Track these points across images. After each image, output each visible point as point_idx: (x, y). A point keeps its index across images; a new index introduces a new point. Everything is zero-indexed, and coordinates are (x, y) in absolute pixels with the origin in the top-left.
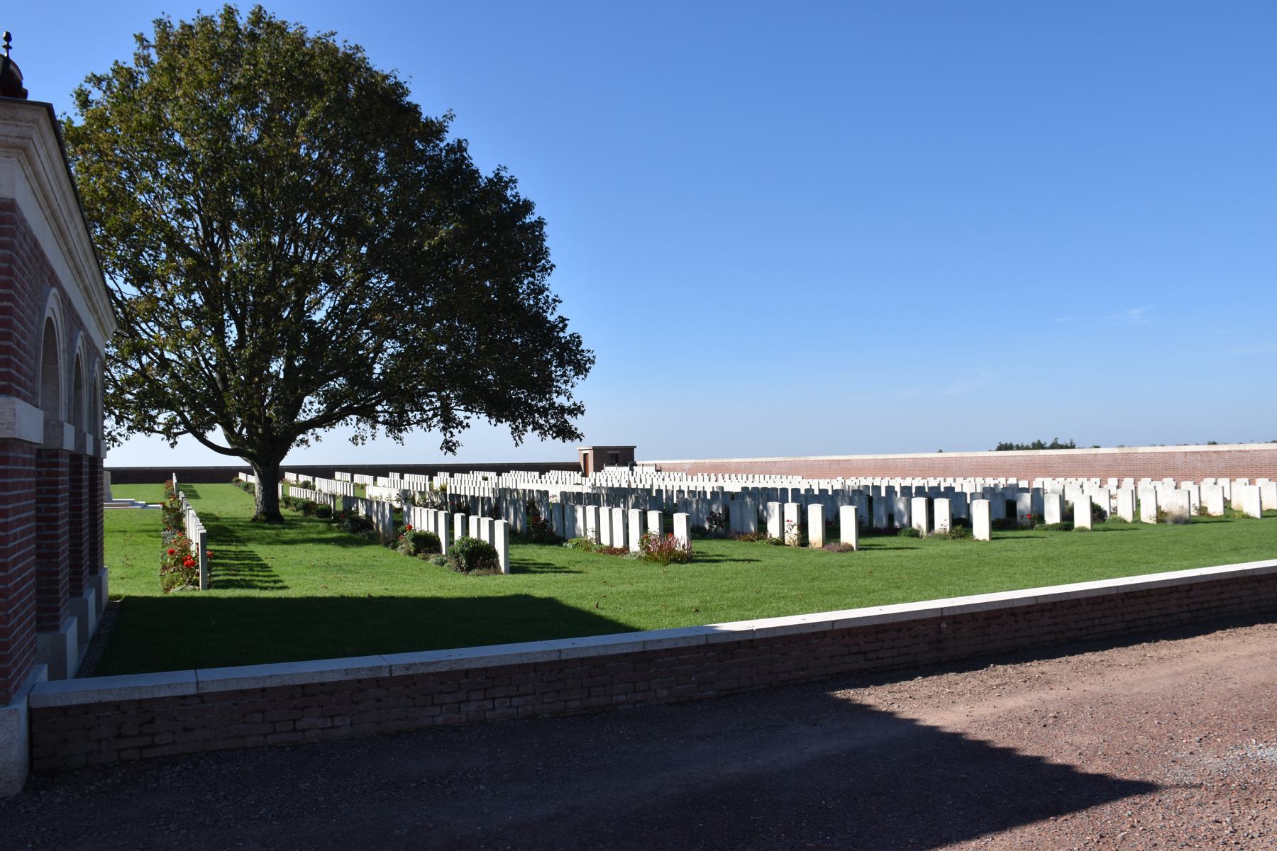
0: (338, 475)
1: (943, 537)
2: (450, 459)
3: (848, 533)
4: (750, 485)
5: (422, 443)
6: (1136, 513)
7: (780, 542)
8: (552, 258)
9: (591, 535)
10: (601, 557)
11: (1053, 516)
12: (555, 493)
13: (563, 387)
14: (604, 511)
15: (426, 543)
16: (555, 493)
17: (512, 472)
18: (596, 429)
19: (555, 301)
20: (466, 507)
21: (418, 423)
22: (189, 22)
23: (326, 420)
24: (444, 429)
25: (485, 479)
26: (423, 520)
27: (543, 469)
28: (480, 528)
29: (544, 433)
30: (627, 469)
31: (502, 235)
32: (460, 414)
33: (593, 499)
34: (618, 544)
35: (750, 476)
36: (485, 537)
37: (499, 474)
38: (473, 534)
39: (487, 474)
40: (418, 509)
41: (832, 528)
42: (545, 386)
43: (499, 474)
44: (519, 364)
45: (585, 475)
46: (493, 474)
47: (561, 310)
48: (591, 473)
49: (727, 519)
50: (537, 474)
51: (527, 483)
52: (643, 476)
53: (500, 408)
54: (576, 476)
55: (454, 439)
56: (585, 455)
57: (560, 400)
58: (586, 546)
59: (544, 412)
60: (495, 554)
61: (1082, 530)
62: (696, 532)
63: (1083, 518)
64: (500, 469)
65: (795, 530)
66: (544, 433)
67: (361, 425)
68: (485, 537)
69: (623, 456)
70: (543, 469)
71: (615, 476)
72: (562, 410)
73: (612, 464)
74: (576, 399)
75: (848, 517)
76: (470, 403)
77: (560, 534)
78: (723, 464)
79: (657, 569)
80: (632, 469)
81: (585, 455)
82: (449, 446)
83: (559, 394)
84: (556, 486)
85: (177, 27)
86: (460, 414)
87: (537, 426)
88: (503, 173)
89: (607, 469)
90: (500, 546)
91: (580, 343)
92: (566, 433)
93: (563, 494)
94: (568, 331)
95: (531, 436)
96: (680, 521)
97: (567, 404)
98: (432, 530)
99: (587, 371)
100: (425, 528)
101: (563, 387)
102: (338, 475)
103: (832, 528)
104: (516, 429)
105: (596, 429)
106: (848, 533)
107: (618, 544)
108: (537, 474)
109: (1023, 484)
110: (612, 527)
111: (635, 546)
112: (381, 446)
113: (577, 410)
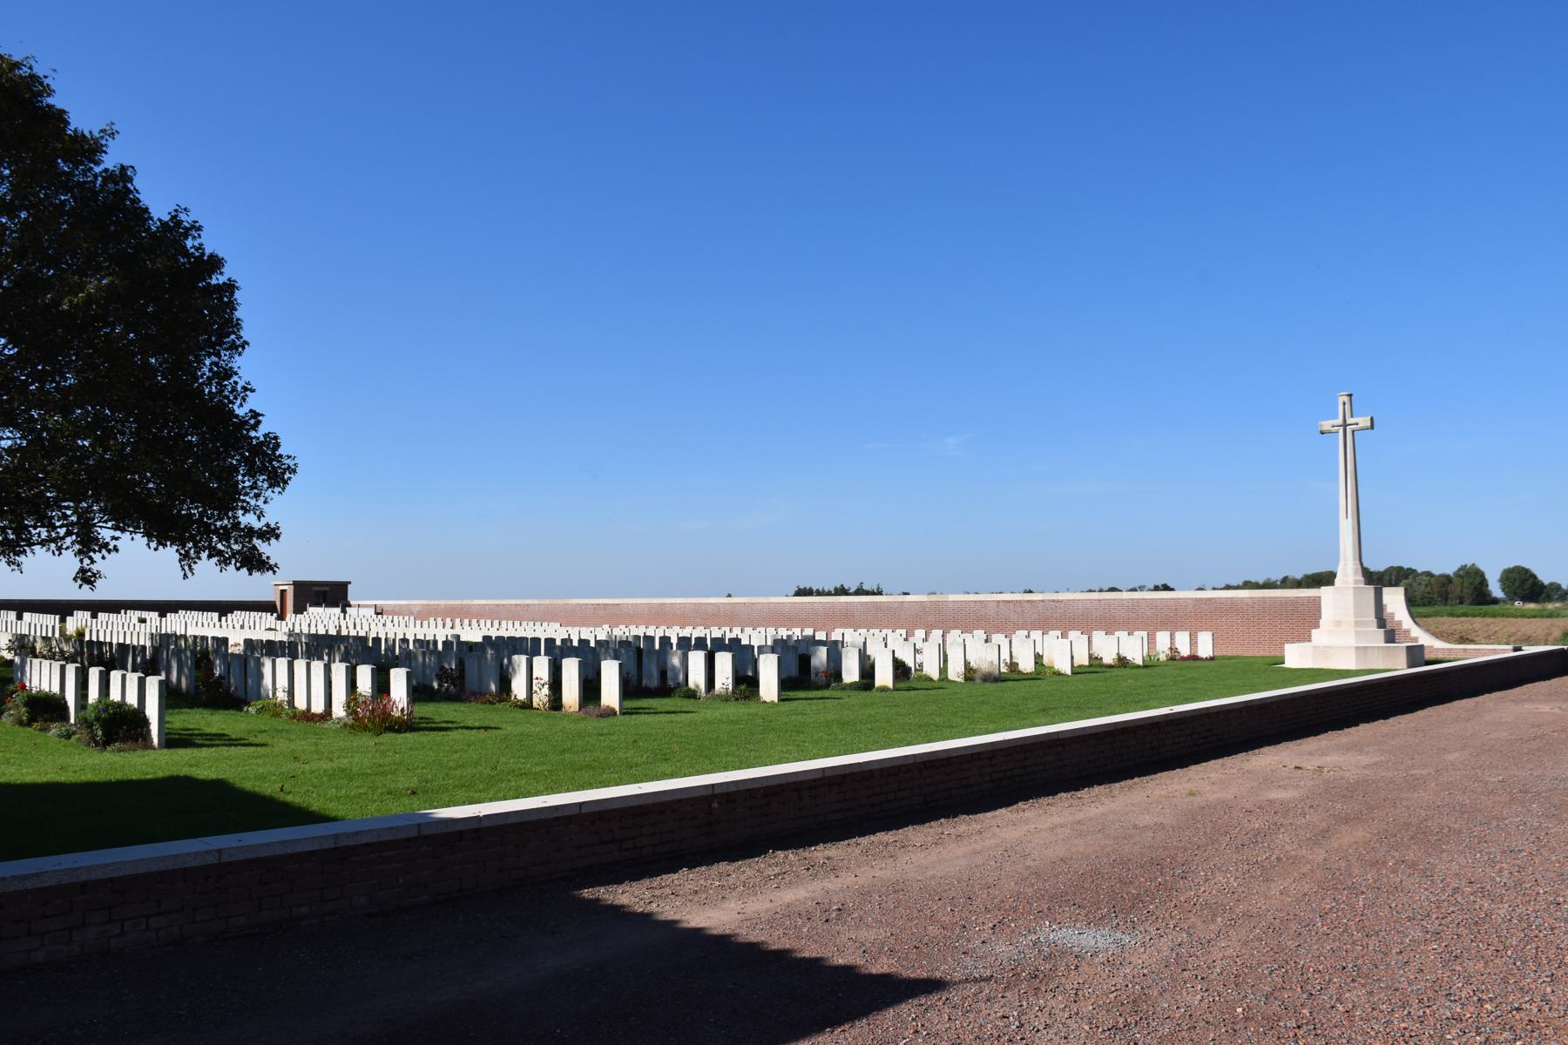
1: (725, 698)
2: (85, 594)
3: (610, 693)
4: (494, 634)
7: (527, 705)
9: (282, 696)
10: (296, 726)
11: (851, 673)
12: (1405, 626)
13: (253, 502)
14: (300, 665)
15: (47, 708)
18: (295, 559)
19: (245, 389)
25: (143, 621)
26: (43, 677)
28: (125, 688)
30: (337, 610)
31: (182, 299)
32: (106, 533)
34: (318, 707)
36: (132, 699)
37: (162, 615)
38: (115, 695)
39: (145, 614)
41: (591, 688)
42: (228, 499)
43: (162, 615)
44: (199, 475)
45: (281, 617)
47: (253, 402)
48: (290, 616)
49: (460, 676)
51: (203, 626)
52: (359, 621)
53: (162, 528)
54: (269, 619)
55: (95, 568)
56: (283, 592)
57: (247, 520)
58: (274, 710)
59: (225, 535)
60: (145, 722)
61: (884, 689)
62: (418, 692)
63: (884, 676)
65: (546, 690)
68: (132, 699)
69: (334, 594)
71: (322, 619)
72: (250, 532)
73: (318, 604)
74: (271, 518)
75: (610, 674)
76: (122, 522)
78: (462, 607)
79: (367, 740)
80: (344, 611)
83: (246, 511)
84: (238, 631)
88: (183, 217)
90: (152, 711)
91: (277, 446)
92: (254, 563)
93: (248, 642)
95: (206, 566)
96: (398, 681)
97: (257, 525)
98: (56, 689)
99: (286, 482)
101: (253, 502)
103: (591, 688)
104: (185, 556)
105: (295, 559)
106: (610, 693)
107: (318, 707)
109: (820, 636)
110: (311, 686)
111: (339, 711)
113: (270, 533)
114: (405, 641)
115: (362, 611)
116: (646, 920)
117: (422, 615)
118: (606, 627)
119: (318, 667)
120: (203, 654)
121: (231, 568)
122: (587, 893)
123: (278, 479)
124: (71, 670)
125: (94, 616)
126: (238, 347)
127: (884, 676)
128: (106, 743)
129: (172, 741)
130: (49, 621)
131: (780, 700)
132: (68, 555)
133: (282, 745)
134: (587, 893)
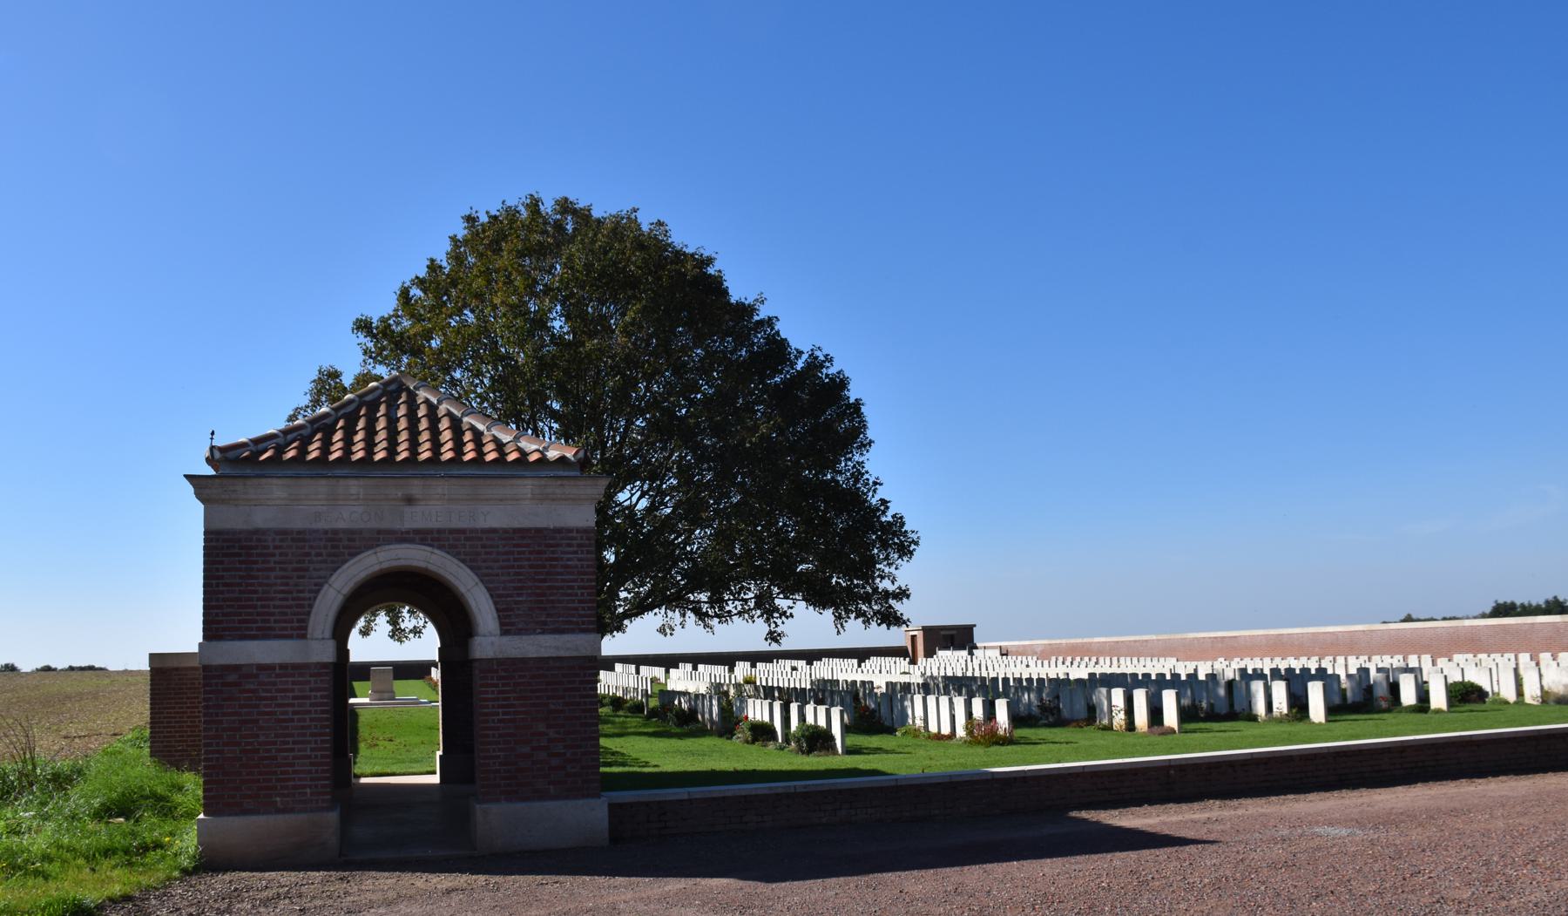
0: (618, 667)
1: (1281, 720)
2: (774, 647)
3: (1171, 717)
4: (1098, 670)
5: (744, 633)
6: (1520, 692)
7: (1109, 728)
8: (870, 434)
9: (919, 723)
10: (931, 743)
11: (1408, 696)
12: (880, 683)
13: (887, 570)
14: (931, 699)
15: (762, 732)
16: (880, 683)
17: (825, 660)
18: (919, 612)
19: (875, 483)
20: (788, 696)
21: (740, 614)
22: (494, 212)
23: (640, 608)
24: (767, 620)
25: (794, 669)
26: (757, 711)
27: (861, 655)
28: (816, 715)
29: (867, 622)
30: (964, 653)
31: (822, 413)
32: (782, 603)
33: (926, 688)
34: (946, 730)
35: (1115, 660)
36: (822, 723)
37: (810, 663)
38: (810, 720)
39: (795, 663)
40: (750, 701)
41: (1156, 713)
42: (867, 569)
43: (810, 663)
44: (840, 547)
45: (913, 662)
46: (801, 664)
47: (882, 493)
48: (921, 660)
49: (1056, 707)
50: (855, 661)
51: (845, 672)
52: (987, 662)
53: (820, 596)
54: (903, 663)
55: (779, 630)
56: (913, 637)
57: (885, 585)
58: (915, 733)
59: (867, 599)
60: (832, 738)
61: (1438, 711)
62: (1016, 719)
63: (1438, 699)
64: (811, 656)
65: (1122, 715)
66: (867, 622)
67: (670, 613)
68: (822, 723)
69: (961, 638)
70: (861, 655)
71: (950, 662)
72: (887, 595)
73: (946, 648)
74: (902, 582)
75: (1169, 699)
76: (787, 593)
77: (887, 723)
78: (1083, 645)
79: (980, 750)
80: (971, 654)
81: (913, 637)
82: (773, 637)
83: (882, 578)
84: (880, 674)
85: (484, 219)
86: (782, 603)
87: (860, 614)
88: (818, 353)
89: (941, 653)
90: (836, 730)
91: (903, 524)
92: (891, 619)
93: (889, 685)
94: (890, 513)
95: (854, 625)
96: (1001, 708)
97: (891, 588)
98: (766, 719)
99: (911, 553)
100: (758, 718)
101: (887, 570)
102: (618, 667)
103: (1156, 713)
104: (839, 618)
105: (919, 612)
106: (1171, 717)
107: (946, 730)
108: (855, 661)
109: (1313, 666)
110: (941, 715)
111: (961, 732)
112: (690, 635)
113: (902, 594)
114: (1006, 680)
115: (988, 653)
116: (1098, 823)
117: (1044, 655)
118: (1174, 660)
119: (944, 700)
120: (854, 699)
121: (874, 624)
122: (1074, 814)
123: (905, 551)
124: (777, 705)
125: (753, 666)
126: (866, 445)
127: (1438, 699)
128: (809, 752)
129: (849, 751)
130: (720, 672)
131: (1327, 721)
132: (760, 622)
133: (922, 752)
134: (1074, 814)
